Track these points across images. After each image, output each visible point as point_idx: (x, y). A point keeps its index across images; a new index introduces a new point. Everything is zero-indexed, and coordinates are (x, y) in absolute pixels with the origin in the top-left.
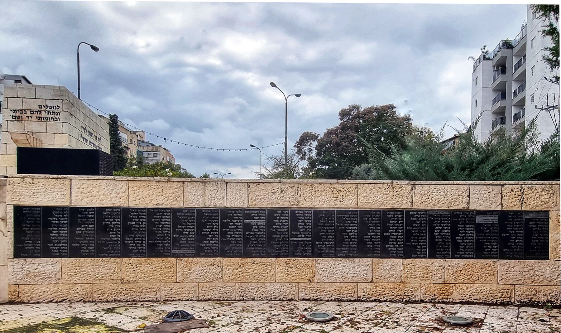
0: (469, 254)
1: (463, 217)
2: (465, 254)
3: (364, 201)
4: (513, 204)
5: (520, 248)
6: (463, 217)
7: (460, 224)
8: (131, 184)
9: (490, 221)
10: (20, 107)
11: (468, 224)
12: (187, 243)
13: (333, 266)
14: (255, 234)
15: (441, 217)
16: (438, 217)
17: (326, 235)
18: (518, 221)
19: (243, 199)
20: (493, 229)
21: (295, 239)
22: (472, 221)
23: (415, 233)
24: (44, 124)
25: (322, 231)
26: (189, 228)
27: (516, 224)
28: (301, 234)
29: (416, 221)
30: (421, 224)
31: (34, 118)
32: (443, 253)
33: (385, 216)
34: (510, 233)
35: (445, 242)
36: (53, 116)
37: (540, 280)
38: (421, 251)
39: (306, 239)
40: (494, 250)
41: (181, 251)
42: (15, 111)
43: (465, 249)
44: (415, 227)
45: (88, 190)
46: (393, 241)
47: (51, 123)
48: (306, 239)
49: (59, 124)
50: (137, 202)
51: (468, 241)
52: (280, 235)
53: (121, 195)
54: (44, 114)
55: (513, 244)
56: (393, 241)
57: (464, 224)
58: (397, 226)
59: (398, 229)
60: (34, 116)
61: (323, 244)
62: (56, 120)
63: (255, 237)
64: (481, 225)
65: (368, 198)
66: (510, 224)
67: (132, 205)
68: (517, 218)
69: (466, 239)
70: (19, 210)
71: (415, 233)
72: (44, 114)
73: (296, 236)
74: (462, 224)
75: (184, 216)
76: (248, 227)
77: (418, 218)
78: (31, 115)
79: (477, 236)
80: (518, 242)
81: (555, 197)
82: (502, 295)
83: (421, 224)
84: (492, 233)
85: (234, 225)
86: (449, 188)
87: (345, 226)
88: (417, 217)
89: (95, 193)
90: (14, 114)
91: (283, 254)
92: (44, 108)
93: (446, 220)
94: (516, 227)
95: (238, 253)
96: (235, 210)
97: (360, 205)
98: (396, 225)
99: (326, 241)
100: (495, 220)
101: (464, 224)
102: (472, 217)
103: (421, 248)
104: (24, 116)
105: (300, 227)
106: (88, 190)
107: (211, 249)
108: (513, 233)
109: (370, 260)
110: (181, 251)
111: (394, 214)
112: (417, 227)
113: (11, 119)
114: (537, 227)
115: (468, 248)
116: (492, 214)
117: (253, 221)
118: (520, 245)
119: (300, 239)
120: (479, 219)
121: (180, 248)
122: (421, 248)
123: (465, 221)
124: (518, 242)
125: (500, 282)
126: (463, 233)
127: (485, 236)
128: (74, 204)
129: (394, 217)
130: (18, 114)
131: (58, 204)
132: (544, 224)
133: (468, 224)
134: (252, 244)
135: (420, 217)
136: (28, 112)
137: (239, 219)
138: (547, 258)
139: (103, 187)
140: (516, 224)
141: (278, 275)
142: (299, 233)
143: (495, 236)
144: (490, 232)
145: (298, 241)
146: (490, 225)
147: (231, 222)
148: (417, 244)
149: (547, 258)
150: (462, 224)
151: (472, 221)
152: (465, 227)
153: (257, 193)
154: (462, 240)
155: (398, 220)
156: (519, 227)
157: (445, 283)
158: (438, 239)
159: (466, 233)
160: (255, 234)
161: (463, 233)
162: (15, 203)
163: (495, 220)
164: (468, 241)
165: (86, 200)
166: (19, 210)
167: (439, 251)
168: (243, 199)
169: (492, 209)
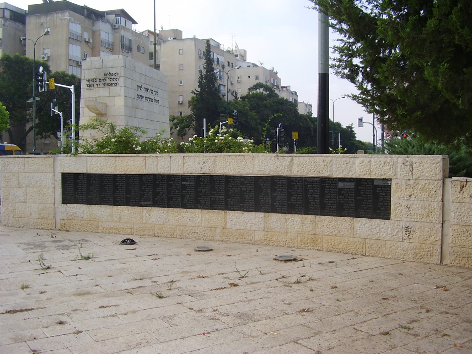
0: (333, 212)
1: (329, 183)
2: (330, 212)
3: (258, 169)
4: (364, 173)
5: (370, 209)
6: (329, 183)
7: (326, 188)
8: (117, 159)
9: (348, 187)
10: (92, 77)
11: (332, 188)
12: (148, 198)
13: (238, 217)
14: (188, 193)
15: (313, 182)
16: (311, 182)
17: (233, 194)
18: (369, 187)
19: (180, 167)
20: (350, 193)
21: (213, 196)
22: (336, 186)
23: (294, 194)
24: (107, 89)
25: (327, 182)
26: (149, 187)
27: (367, 189)
28: (217, 193)
29: (295, 185)
30: (298, 187)
31: (102, 85)
32: (315, 211)
33: (273, 181)
34: (363, 197)
35: (315, 202)
36: (114, 82)
37: (384, 236)
38: (298, 209)
39: (220, 197)
40: (351, 210)
41: (145, 203)
42: (89, 81)
43: (330, 208)
44: (294, 189)
45: (96, 163)
46: (279, 200)
47: (113, 88)
48: (220, 197)
49: (117, 88)
50: (120, 170)
51: (332, 202)
52: (204, 193)
53: (112, 166)
54: (108, 81)
55: (365, 206)
56: (279, 200)
57: (330, 188)
58: (282, 189)
59: (282, 191)
60: (101, 83)
61: (232, 201)
62: (116, 84)
63: (188, 195)
64: (342, 189)
65: (260, 167)
66: (363, 189)
67: (118, 173)
68: (368, 184)
69: (331, 200)
70: (64, 176)
71: (294, 194)
72: (108, 81)
73: (214, 194)
74: (328, 188)
75: (146, 179)
76: (184, 187)
77: (296, 183)
78: (100, 83)
79: (339, 198)
80: (369, 204)
81: (394, 168)
82: (356, 246)
83: (298, 187)
84: (350, 196)
85: (176, 186)
86: (317, 159)
87: (246, 188)
88: (295, 182)
89: (99, 165)
90: (89, 84)
91: (206, 207)
92: (108, 76)
93: (317, 185)
94: (367, 192)
95: (178, 205)
96: (176, 176)
97: (256, 172)
98: (281, 188)
99: (234, 198)
100: (352, 185)
101: (330, 188)
102: (335, 183)
103: (298, 206)
104: (95, 84)
105: (216, 188)
106: (96, 163)
107: (162, 202)
108: (365, 197)
109: (262, 214)
110: (145, 203)
111: (280, 180)
112: (296, 190)
113: (86, 87)
114: (382, 192)
115: (333, 208)
116: (350, 181)
117: (187, 183)
118: (370, 207)
119: (217, 197)
120: (341, 185)
121: (144, 201)
122: (298, 206)
123: (330, 186)
124: (369, 204)
125: (356, 236)
126: (329, 196)
127: (345, 198)
128: (89, 172)
129: (279, 181)
130: (91, 83)
131: (81, 172)
132: (387, 190)
133: (332, 188)
134: (187, 199)
135: (298, 182)
136: (98, 80)
137: (178, 182)
138: (389, 218)
139: (103, 161)
140: (367, 189)
141: (203, 222)
142: (215, 192)
143: (352, 198)
144: (348, 196)
145: (216, 198)
146: (348, 190)
147: (174, 183)
148: (295, 203)
149: (389, 218)
150: (328, 188)
151: (336, 186)
152: (330, 191)
153: (189, 164)
154: (328, 200)
155: (282, 184)
156: (370, 192)
157: (315, 234)
158: (311, 199)
159: (331, 195)
160: (188, 193)
161: (329, 196)
162: (62, 172)
163: (352, 185)
164: (332, 202)
165: (95, 169)
166: (64, 176)
167: (311, 209)
168: (180, 167)
169: (349, 177)
